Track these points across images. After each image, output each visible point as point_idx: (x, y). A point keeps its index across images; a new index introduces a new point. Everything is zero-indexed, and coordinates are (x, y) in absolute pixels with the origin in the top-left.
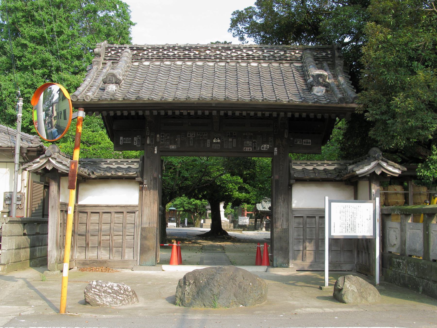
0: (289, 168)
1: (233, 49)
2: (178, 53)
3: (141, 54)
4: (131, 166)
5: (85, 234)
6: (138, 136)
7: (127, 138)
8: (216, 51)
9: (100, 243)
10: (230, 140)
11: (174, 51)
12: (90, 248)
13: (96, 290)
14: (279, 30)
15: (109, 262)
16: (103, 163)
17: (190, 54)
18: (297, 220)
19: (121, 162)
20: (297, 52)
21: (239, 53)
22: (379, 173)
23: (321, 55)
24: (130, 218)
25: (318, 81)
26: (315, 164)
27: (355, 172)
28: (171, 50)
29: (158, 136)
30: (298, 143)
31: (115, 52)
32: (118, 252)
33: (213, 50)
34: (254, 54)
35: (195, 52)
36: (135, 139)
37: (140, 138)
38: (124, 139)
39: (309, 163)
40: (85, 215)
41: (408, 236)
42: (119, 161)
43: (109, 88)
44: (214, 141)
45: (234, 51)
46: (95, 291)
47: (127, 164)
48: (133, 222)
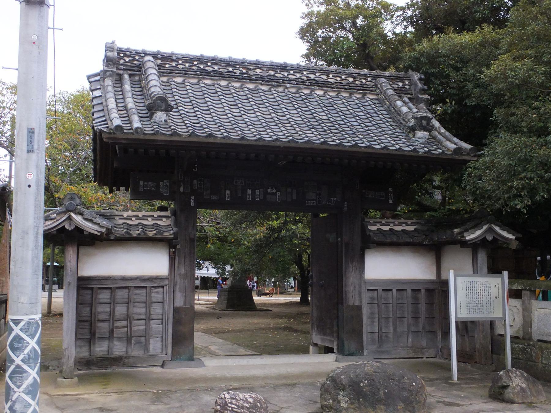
0: (364, 229)
1: (291, 70)
2: (219, 69)
3: (167, 66)
4: (159, 222)
5: (89, 319)
6: (165, 181)
7: (150, 183)
8: (268, 70)
9: (111, 332)
10: (289, 190)
11: (213, 66)
12: (96, 340)
13: (233, 406)
14: (350, 50)
15: (126, 358)
16: (117, 218)
17: (235, 71)
18: (370, 294)
19: (143, 216)
20: (369, 79)
21: (298, 75)
22: (490, 238)
23: (397, 86)
24: (157, 295)
25: (421, 124)
26: (391, 223)
27: (465, 237)
28: (209, 64)
29: (195, 182)
30: (370, 196)
31: (131, 59)
32: (139, 343)
33: (265, 69)
34: (316, 79)
35: (241, 69)
36: (161, 184)
37: (168, 184)
38: (146, 183)
39: (384, 222)
40: (89, 292)
41: (536, 317)
42: (140, 214)
43: (156, 117)
44: (269, 191)
45: (292, 72)
46: (232, 408)
47: (152, 220)
48: (161, 301)
